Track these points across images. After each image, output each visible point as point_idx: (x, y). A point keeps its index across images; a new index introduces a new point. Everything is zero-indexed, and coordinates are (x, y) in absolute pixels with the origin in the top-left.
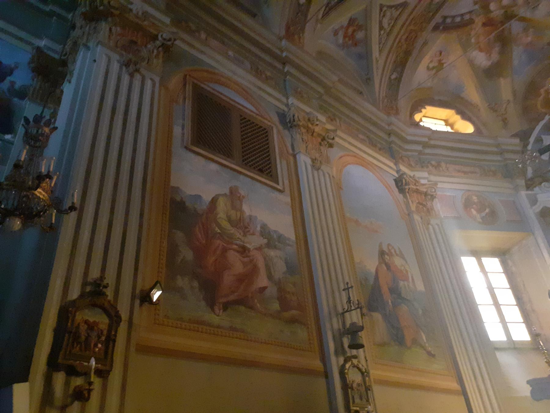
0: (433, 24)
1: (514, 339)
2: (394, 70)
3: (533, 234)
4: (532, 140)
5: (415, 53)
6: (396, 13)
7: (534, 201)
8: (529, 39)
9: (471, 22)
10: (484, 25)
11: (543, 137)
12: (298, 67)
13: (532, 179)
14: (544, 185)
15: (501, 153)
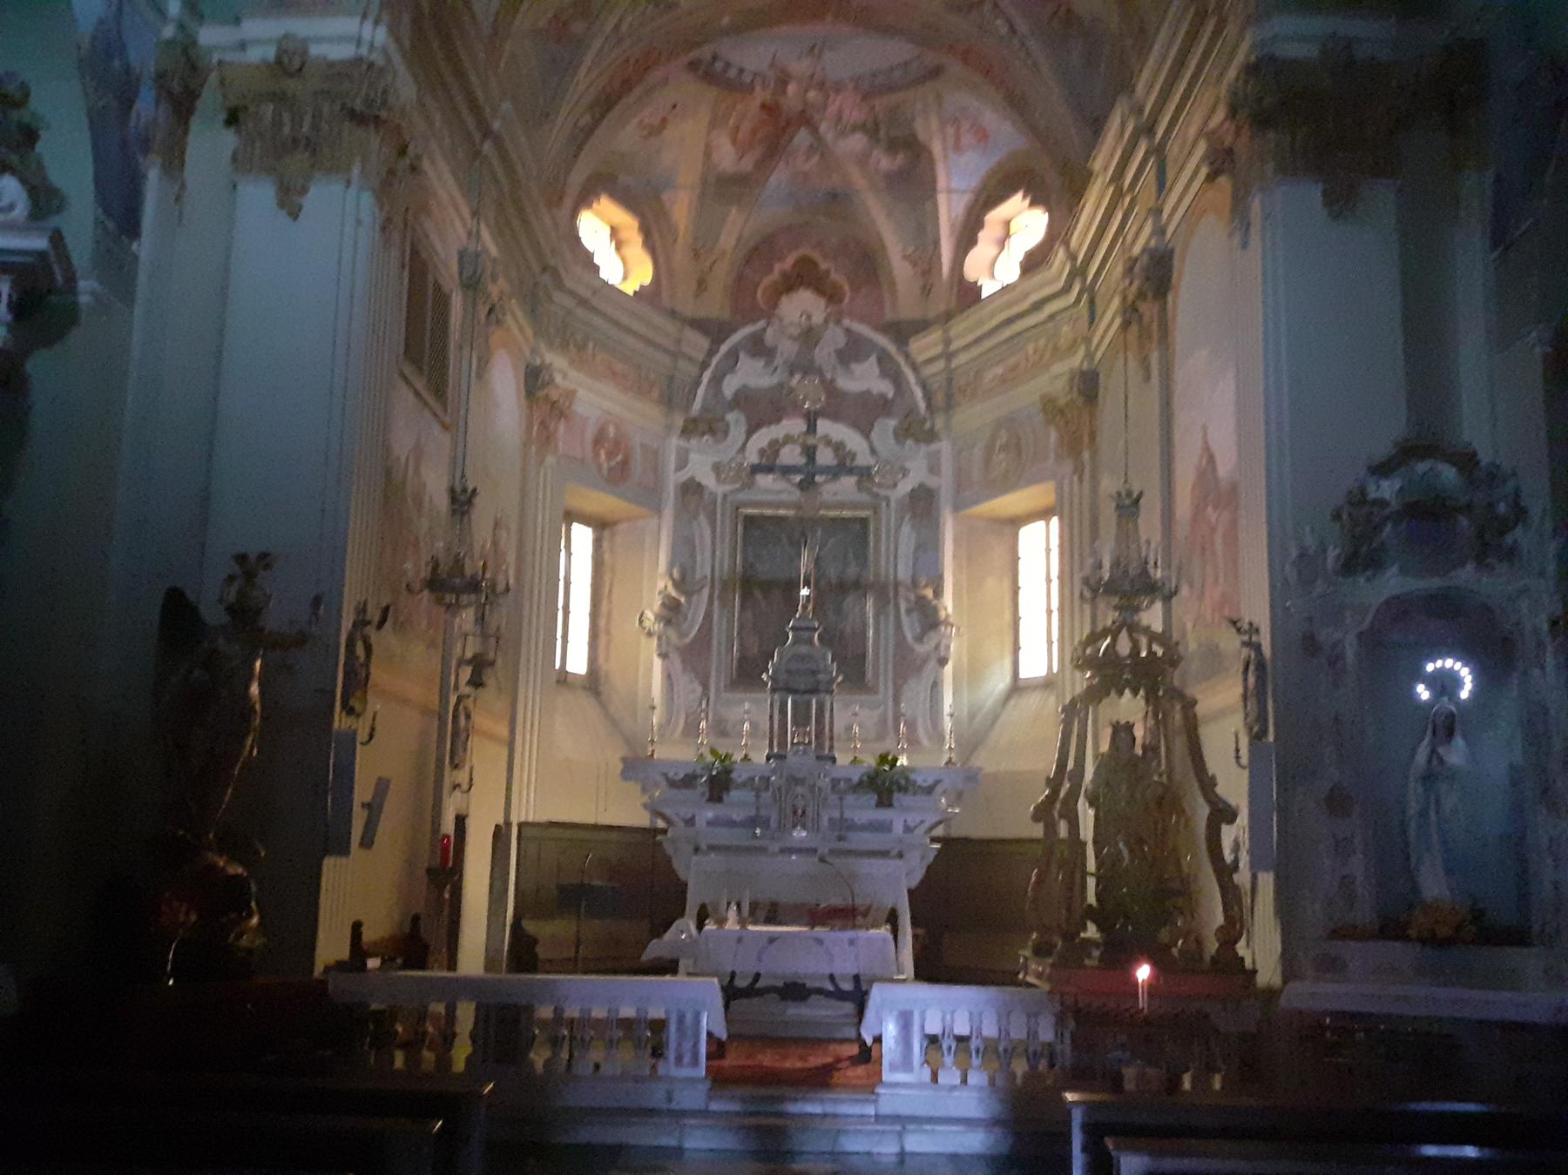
0: (694, 54)
1: (567, 669)
2: (591, 107)
3: (660, 517)
4: (724, 348)
7: (682, 464)
8: (807, 167)
11: (742, 356)
12: (504, 157)
13: (695, 420)
14: (707, 441)
15: (675, 355)
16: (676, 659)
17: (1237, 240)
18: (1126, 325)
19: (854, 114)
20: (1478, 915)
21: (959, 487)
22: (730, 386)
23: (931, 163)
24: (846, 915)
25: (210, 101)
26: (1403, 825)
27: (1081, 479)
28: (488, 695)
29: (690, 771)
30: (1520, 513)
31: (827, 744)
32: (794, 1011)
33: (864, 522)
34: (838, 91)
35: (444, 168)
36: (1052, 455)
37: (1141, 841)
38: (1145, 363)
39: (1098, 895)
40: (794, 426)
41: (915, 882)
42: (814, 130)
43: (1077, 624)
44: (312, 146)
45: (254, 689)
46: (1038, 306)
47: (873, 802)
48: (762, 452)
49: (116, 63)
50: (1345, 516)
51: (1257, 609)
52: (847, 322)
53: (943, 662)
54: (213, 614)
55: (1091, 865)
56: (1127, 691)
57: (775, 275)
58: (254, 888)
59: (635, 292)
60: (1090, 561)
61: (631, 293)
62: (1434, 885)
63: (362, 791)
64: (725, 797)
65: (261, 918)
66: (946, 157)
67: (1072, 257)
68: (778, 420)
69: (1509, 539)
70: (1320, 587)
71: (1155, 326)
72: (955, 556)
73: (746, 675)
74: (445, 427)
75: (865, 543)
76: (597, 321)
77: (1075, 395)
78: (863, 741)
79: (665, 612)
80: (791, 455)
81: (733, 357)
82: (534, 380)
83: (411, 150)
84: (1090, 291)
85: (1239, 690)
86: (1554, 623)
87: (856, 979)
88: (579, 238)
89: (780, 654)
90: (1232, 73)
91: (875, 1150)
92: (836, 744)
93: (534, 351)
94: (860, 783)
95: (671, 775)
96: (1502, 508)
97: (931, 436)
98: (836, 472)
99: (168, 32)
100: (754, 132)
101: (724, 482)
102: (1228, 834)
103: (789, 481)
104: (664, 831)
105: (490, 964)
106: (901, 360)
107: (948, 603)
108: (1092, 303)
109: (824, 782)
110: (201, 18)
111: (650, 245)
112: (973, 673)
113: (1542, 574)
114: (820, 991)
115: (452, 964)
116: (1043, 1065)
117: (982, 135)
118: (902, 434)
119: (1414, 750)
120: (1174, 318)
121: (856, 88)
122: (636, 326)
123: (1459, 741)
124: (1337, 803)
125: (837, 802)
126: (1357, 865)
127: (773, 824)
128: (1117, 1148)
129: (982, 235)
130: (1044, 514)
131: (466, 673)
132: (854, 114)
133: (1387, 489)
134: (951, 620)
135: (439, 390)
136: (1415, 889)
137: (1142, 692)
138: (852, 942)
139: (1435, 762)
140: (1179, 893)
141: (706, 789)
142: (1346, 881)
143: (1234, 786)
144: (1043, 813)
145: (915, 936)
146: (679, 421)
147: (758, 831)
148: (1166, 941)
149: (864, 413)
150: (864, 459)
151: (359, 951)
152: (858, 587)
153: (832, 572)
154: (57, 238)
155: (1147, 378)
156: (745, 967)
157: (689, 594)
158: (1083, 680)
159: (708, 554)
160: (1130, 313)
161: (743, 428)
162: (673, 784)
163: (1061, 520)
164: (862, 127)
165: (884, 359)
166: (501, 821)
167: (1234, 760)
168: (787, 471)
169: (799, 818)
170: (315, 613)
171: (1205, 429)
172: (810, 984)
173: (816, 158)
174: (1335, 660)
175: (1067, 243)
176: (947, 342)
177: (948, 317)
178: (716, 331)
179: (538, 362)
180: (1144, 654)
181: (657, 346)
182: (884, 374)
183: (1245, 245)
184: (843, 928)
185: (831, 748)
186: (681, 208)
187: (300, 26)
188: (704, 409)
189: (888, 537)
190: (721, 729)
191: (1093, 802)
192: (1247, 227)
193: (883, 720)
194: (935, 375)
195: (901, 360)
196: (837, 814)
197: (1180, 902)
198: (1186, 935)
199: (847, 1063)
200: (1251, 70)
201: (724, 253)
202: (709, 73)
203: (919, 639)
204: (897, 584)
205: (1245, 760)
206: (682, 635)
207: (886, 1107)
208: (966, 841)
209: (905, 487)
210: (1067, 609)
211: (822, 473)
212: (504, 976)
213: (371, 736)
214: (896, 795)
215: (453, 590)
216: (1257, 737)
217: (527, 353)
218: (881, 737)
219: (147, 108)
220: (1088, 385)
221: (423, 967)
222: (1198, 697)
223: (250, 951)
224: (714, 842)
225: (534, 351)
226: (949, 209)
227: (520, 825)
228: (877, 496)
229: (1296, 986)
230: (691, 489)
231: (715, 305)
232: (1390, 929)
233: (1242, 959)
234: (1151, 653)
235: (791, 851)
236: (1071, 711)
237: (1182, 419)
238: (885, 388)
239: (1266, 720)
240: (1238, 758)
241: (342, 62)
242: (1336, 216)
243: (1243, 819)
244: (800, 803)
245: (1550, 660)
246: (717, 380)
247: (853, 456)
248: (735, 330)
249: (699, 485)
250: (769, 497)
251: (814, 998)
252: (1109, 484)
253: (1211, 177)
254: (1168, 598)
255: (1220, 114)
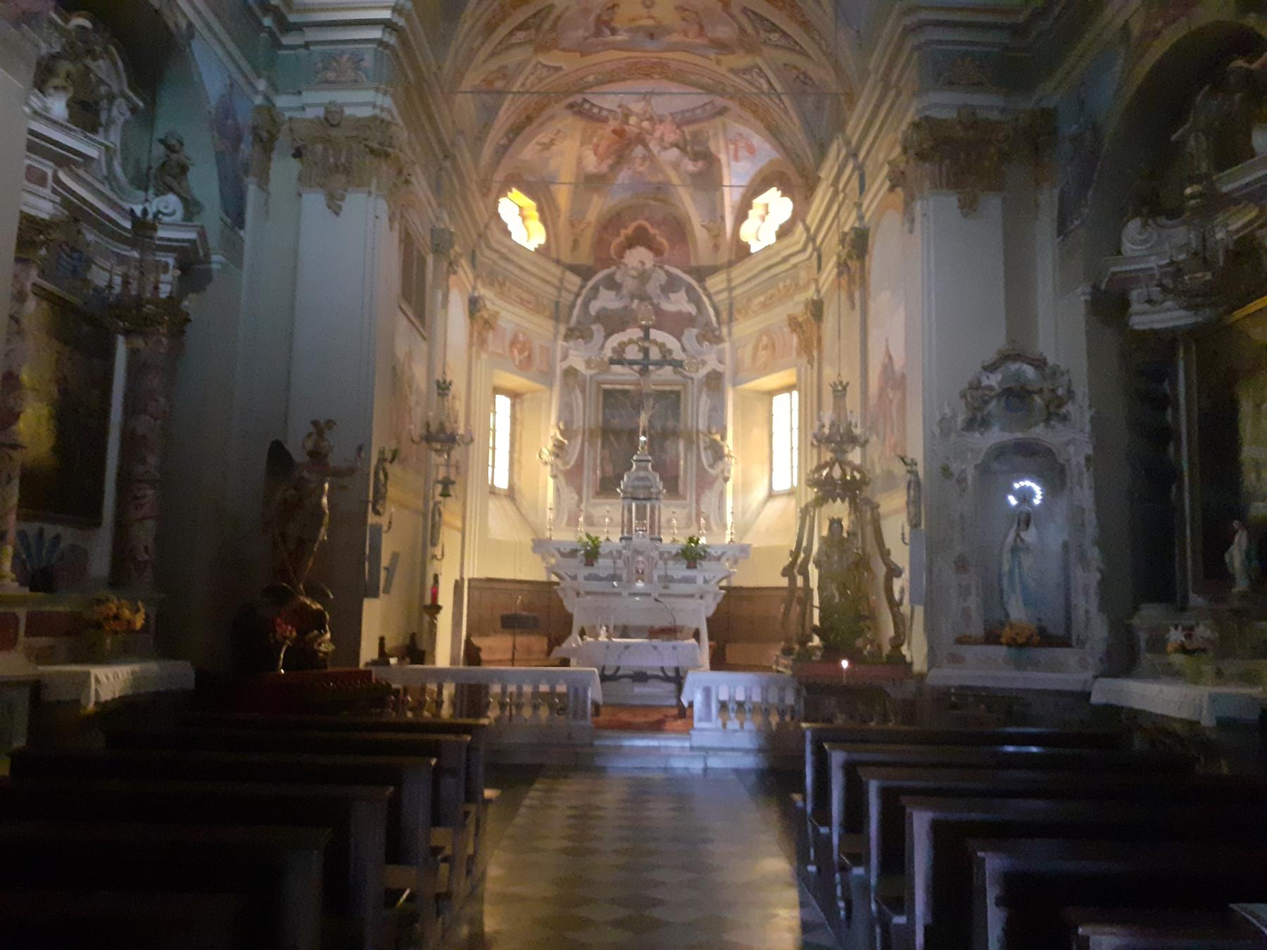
0: (571, 100)
2: (506, 135)
4: (590, 284)
5: (535, 124)
6: (545, 72)
7: (565, 357)
8: (642, 169)
9: (605, 120)
10: (614, 131)
11: (601, 288)
16: (562, 479)
17: (907, 226)
18: (840, 274)
19: (671, 137)
20: (1042, 631)
21: (735, 373)
22: (594, 307)
23: (720, 169)
24: (670, 632)
25: (284, 142)
26: (1000, 576)
27: (812, 366)
28: (449, 501)
29: (574, 547)
30: (1070, 394)
31: (657, 530)
32: (639, 689)
33: (678, 394)
34: (661, 122)
35: (422, 178)
36: (794, 352)
37: (845, 587)
38: (851, 297)
39: (821, 619)
40: (634, 333)
41: (710, 612)
42: (646, 146)
43: (809, 459)
44: (347, 171)
45: (325, 500)
46: (785, 259)
47: (684, 566)
48: (614, 350)
49: (230, 121)
50: (968, 395)
51: (916, 451)
52: (666, 267)
53: (726, 480)
54: (299, 456)
55: (816, 602)
56: (839, 500)
57: (622, 238)
58: (328, 617)
59: (536, 249)
60: (817, 424)
61: (533, 250)
62: (1017, 612)
63: (385, 561)
64: (595, 564)
65: (332, 635)
66: (729, 165)
67: (807, 229)
68: (623, 330)
69: (1063, 410)
70: (953, 437)
71: (857, 276)
72: (734, 414)
73: (607, 487)
74: (424, 338)
75: (679, 407)
76: (510, 267)
77: (809, 315)
78: (678, 528)
79: (556, 451)
80: (632, 353)
81: (595, 290)
82: (474, 305)
83: (405, 172)
84: (818, 250)
85: (905, 499)
86: (1088, 459)
87: (677, 670)
88: (499, 215)
89: (629, 477)
90: (904, 126)
91: (690, 766)
92: (662, 531)
93: (474, 288)
94: (677, 554)
95: (562, 550)
96: (1060, 392)
97: (719, 339)
98: (660, 364)
99: (259, 100)
100: (609, 147)
101: (592, 368)
102: (897, 584)
103: (632, 369)
104: (557, 584)
105: (454, 660)
106: (700, 291)
107: (729, 444)
108: (819, 257)
109: (655, 554)
110: (277, 91)
111: (543, 220)
112: (745, 488)
113: (1082, 431)
114: (656, 677)
115: (433, 662)
116: (788, 718)
117: (752, 150)
118: (701, 338)
119: (1006, 536)
120: (869, 273)
121: (673, 120)
122: (534, 269)
123: (1032, 529)
124: (961, 565)
125: (663, 566)
126: (973, 602)
127: (624, 576)
128: (830, 748)
129: (751, 212)
130: (789, 389)
131: (439, 488)
132: (671, 137)
133: (994, 380)
134: (732, 454)
135: (421, 315)
136: (1007, 615)
137: (847, 499)
138: (674, 648)
139: (1018, 540)
140: (866, 618)
141: (583, 558)
142: (966, 613)
143: (901, 555)
144: (787, 572)
145: (710, 647)
146: (563, 329)
147: (615, 583)
148: (861, 645)
149: (677, 324)
150: (678, 355)
151: (383, 655)
152: (675, 434)
153: (658, 426)
154: (202, 234)
155: (853, 307)
156: (611, 663)
157: (569, 439)
158: (812, 494)
159: (581, 412)
160: (842, 267)
161: (603, 334)
162: (563, 555)
163: (800, 394)
164: (677, 145)
165: (690, 290)
166: (458, 578)
167: (901, 541)
168: (631, 363)
169: (640, 575)
170: (359, 455)
171: (887, 340)
172: (649, 673)
173: (647, 163)
174: (961, 481)
175: (804, 221)
176: (729, 280)
177: (730, 264)
178: (585, 273)
179: (476, 294)
180: (848, 478)
181: (548, 282)
182: (690, 300)
183: (911, 232)
184: (669, 640)
185: (659, 533)
186: (563, 196)
187: (340, 96)
188: (579, 322)
189: (693, 403)
190: (590, 522)
191: (818, 564)
192: (912, 221)
193: (689, 518)
194: (723, 300)
195: (700, 291)
196: (662, 573)
197: (868, 622)
198: (872, 642)
199: (672, 719)
200: (916, 126)
201: (589, 224)
202: (578, 110)
203: (712, 466)
204: (698, 431)
205: (907, 540)
206: (566, 463)
207: (696, 743)
208: (741, 589)
209: (703, 372)
210: (803, 448)
211: (652, 364)
212: (461, 667)
213: (389, 527)
214: (698, 561)
215: (438, 441)
216: (915, 526)
217: (470, 289)
218: (688, 526)
219: (246, 148)
220: (817, 309)
221: (422, 663)
222: (881, 503)
223: (325, 653)
224: (588, 589)
225: (474, 288)
226: (730, 198)
227: (470, 580)
228: (685, 377)
229: (934, 672)
230: (570, 373)
231: (584, 257)
232: (991, 638)
233: (904, 657)
234: (853, 477)
235: (635, 594)
236: (805, 512)
237: (873, 333)
238: (691, 309)
239: (920, 517)
240: (903, 539)
241: (365, 119)
242: (965, 216)
243: (906, 575)
244: (641, 566)
245: (1085, 482)
246: (586, 305)
247: (670, 352)
248: (596, 272)
249: (575, 370)
250: (618, 378)
251: (650, 682)
252: (829, 374)
253: (892, 189)
254: (864, 445)
255: (898, 150)
